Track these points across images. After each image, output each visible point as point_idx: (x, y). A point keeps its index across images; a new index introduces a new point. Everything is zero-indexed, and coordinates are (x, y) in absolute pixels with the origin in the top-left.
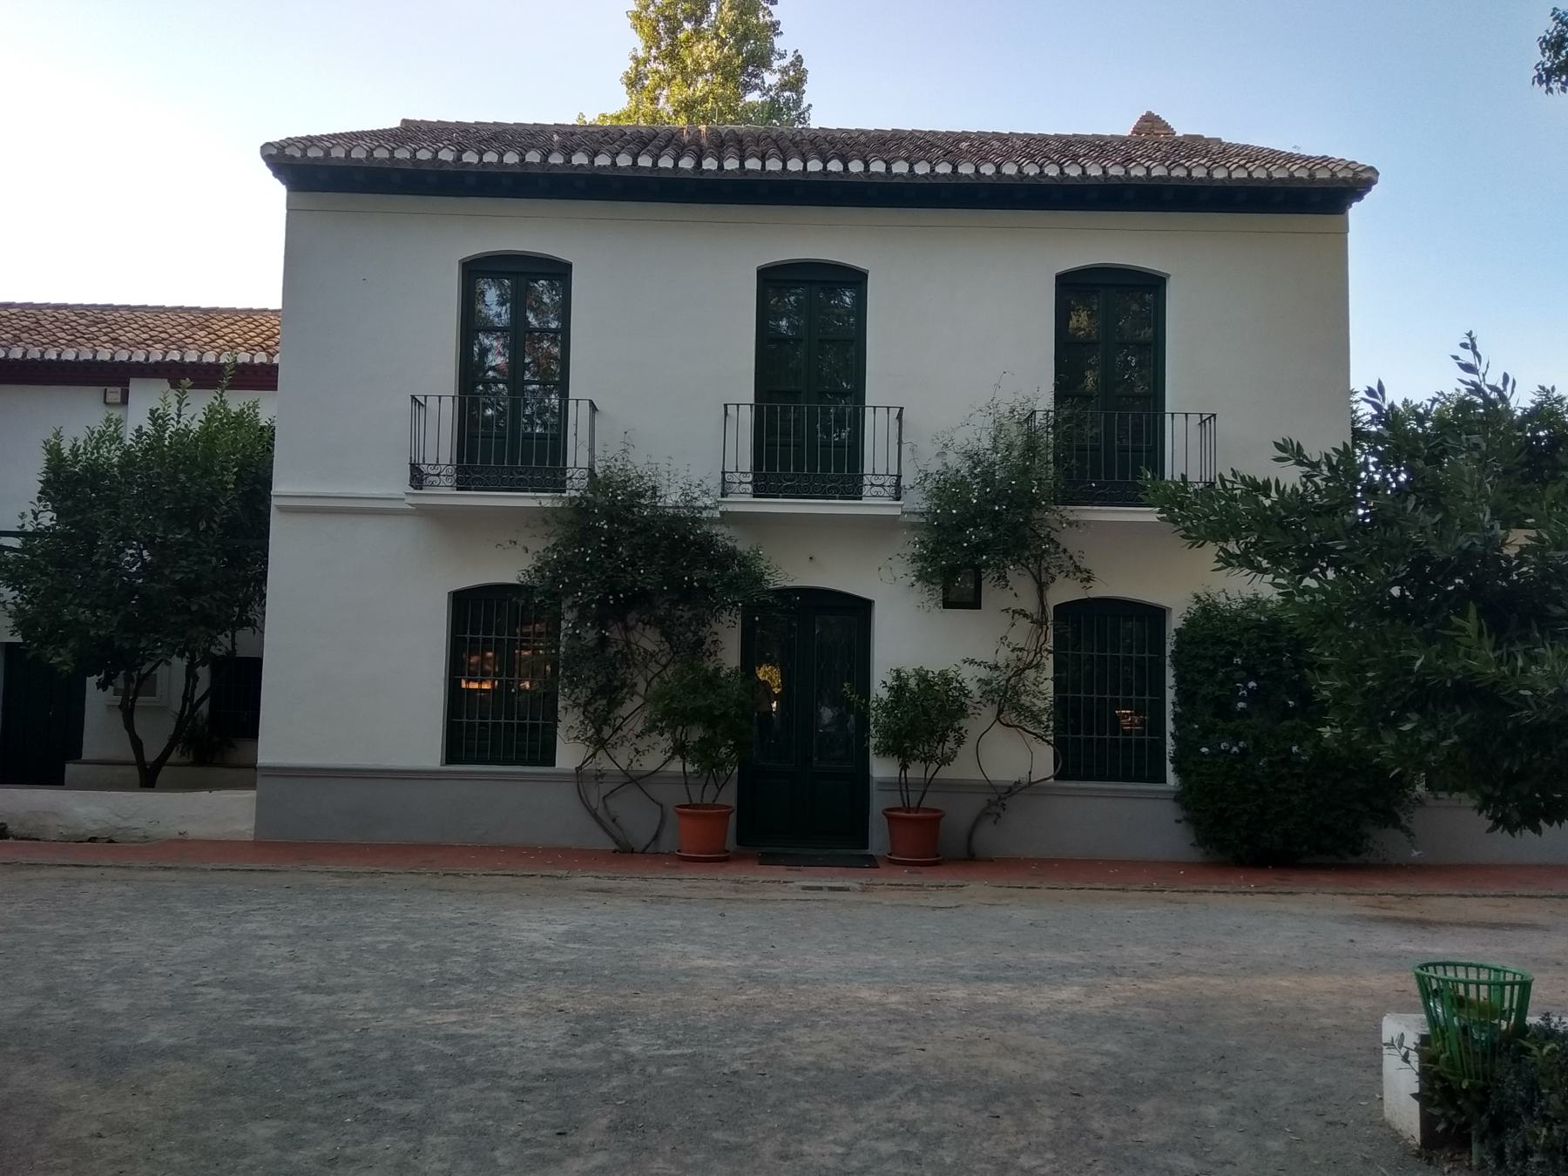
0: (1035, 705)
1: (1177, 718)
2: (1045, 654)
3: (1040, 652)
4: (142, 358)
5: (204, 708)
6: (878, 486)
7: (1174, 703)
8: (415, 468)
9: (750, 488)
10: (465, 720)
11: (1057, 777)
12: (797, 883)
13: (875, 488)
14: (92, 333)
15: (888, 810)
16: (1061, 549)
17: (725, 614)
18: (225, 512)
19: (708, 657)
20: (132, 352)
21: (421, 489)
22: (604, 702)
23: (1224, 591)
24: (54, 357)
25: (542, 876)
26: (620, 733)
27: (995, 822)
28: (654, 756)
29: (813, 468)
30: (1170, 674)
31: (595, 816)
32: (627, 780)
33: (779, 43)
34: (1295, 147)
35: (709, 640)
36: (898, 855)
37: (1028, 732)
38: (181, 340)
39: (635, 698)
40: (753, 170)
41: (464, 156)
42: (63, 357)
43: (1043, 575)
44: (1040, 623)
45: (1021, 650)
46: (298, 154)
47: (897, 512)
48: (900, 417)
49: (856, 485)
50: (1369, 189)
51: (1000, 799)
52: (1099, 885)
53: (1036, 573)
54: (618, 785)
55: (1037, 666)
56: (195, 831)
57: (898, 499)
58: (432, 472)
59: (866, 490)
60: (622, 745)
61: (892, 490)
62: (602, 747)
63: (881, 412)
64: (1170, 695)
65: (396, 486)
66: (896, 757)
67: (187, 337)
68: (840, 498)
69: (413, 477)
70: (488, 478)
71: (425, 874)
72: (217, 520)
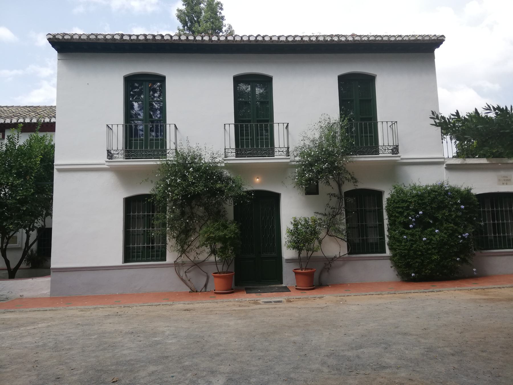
5: (34, 247)
6: (281, 152)
8: (109, 152)
11: (348, 254)
15: (294, 270)
17: (228, 200)
18: (36, 172)
19: (222, 217)
20: (6, 120)
21: (112, 159)
22: (184, 236)
23: (403, 184)
25: (163, 305)
26: (191, 247)
27: (328, 271)
29: (257, 146)
30: (385, 216)
31: (182, 279)
34: (414, 32)
35: (222, 211)
36: (299, 287)
37: (339, 238)
38: (25, 116)
41: (124, 37)
44: (340, 198)
45: (334, 208)
46: (61, 38)
47: (288, 161)
50: (442, 43)
51: (329, 263)
52: (372, 293)
54: (191, 267)
56: (26, 294)
57: (289, 156)
58: (115, 153)
59: (276, 154)
63: (281, 125)
64: (386, 222)
65: (102, 159)
67: (27, 115)
68: (268, 157)
69: (108, 155)
72: (33, 175)
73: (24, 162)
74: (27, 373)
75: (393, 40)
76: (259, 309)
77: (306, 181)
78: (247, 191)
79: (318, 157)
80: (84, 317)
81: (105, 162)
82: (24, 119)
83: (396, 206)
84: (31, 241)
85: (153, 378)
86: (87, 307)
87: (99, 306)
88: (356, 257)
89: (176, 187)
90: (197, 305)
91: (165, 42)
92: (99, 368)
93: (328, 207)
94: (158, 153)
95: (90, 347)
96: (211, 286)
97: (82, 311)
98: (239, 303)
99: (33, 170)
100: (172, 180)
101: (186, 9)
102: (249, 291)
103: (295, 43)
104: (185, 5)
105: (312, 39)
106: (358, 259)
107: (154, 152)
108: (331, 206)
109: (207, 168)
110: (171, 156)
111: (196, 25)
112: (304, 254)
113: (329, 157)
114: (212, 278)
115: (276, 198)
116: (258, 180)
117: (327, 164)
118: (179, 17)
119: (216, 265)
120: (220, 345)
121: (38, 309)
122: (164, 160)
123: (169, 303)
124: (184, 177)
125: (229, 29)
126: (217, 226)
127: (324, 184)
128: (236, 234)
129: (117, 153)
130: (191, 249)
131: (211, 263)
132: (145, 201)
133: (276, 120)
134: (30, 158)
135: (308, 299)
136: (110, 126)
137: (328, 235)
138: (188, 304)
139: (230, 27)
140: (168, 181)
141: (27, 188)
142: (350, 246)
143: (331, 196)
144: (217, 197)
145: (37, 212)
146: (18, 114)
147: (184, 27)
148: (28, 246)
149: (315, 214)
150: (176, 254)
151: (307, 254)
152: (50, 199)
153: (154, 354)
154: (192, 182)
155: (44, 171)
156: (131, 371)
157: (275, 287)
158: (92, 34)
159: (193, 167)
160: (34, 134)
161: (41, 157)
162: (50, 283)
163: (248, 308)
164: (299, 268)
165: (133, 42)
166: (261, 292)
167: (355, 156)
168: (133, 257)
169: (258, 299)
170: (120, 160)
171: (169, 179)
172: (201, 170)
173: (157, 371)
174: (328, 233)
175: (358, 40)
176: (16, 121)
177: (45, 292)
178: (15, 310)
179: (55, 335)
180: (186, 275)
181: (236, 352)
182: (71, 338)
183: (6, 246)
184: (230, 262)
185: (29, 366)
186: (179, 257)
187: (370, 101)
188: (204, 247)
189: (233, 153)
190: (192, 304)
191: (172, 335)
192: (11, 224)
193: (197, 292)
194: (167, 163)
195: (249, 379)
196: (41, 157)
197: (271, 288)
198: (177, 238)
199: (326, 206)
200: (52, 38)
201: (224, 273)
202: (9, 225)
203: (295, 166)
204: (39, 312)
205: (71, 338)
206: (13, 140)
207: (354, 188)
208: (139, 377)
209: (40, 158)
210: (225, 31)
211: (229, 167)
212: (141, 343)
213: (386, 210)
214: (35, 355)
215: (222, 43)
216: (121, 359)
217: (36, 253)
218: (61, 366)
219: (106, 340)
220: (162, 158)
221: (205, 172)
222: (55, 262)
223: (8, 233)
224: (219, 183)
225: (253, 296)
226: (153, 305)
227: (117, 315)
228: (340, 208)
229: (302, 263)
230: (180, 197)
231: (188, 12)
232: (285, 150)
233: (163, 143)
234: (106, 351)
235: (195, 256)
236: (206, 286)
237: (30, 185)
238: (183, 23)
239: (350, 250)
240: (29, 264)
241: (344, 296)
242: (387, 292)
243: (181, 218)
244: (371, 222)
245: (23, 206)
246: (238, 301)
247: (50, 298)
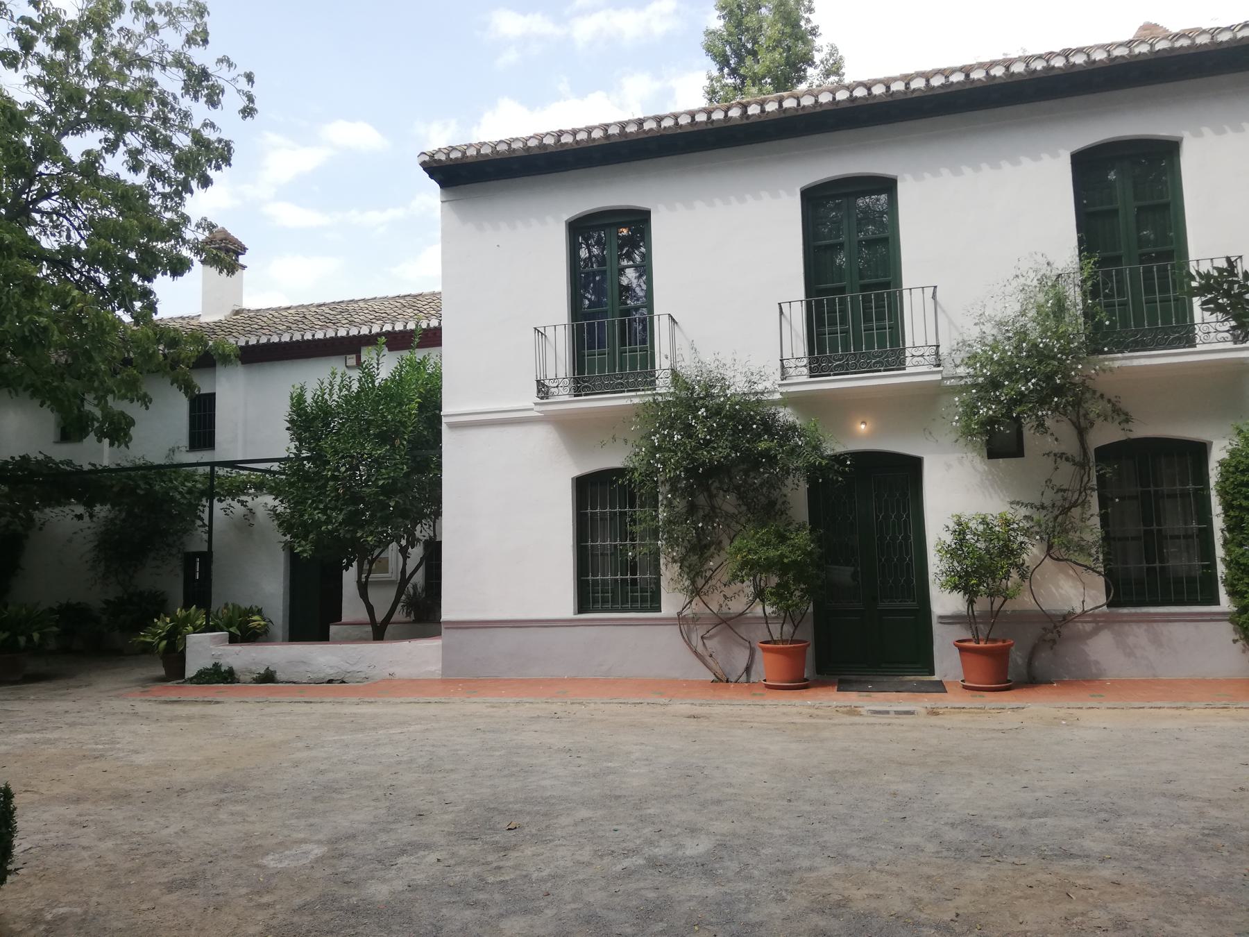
1: (1226, 543)
2: (1089, 492)
3: (1085, 489)
4: (367, 332)
7: (1222, 531)
9: (805, 371)
12: (868, 708)
14: (337, 319)
16: (1098, 394)
18: (412, 432)
21: (547, 398)
24: (310, 338)
31: (696, 653)
33: (818, 42)
35: (780, 502)
38: (394, 317)
40: (790, 108)
41: (562, 138)
42: (316, 337)
43: (1082, 420)
44: (1082, 465)
45: (1064, 491)
46: (443, 158)
47: (938, 377)
48: (934, 296)
51: (1055, 627)
52: (1159, 704)
55: (1084, 503)
56: (401, 672)
57: (939, 365)
58: (552, 385)
59: (908, 360)
60: (712, 593)
61: (932, 359)
62: (698, 594)
64: (1218, 523)
65: (527, 400)
66: (962, 592)
68: (885, 370)
69: (539, 391)
71: (556, 703)
72: (406, 437)
73: (390, 413)
74: (373, 803)
75: (1227, 41)
76: (851, 724)
77: (982, 424)
79: (1011, 364)
80: (492, 717)
81: (532, 406)
83: (1243, 481)
84: (411, 564)
85: (580, 828)
86: (503, 700)
87: (525, 699)
91: (646, 136)
98: (812, 711)
99: (406, 428)
100: (665, 436)
101: (724, 25)
102: (844, 686)
103: (949, 90)
104: (724, 18)
105: (993, 72)
106: (1135, 618)
107: (627, 378)
108: (1058, 485)
109: (737, 407)
110: (663, 385)
111: (749, 61)
112: (982, 604)
113: (1040, 362)
114: (759, 655)
116: (863, 426)
117: (1033, 381)
118: (709, 50)
119: (767, 623)
120: (731, 785)
121: (416, 700)
123: (662, 700)
124: (688, 431)
125: (831, 55)
126: (765, 538)
128: (811, 553)
130: (714, 588)
132: (613, 482)
133: (907, 281)
134: (400, 404)
135: (983, 711)
138: (701, 705)
139: (834, 51)
140: (656, 439)
141: (395, 464)
143: (1059, 459)
144: (762, 470)
146: (383, 315)
147: (721, 70)
148: (404, 580)
149: (1013, 506)
150: (682, 598)
151: (992, 603)
152: (437, 484)
154: (704, 439)
156: (545, 815)
158: (501, 141)
159: (706, 407)
160: (406, 354)
161: (420, 400)
164: (970, 637)
166: (874, 689)
167: (1119, 355)
168: (595, 601)
170: (564, 401)
171: (658, 436)
172: (724, 412)
173: (590, 818)
174: (1051, 552)
175: (1121, 56)
177: (433, 668)
178: (377, 699)
179: (433, 746)
181: (758, 800)
182: (459, 752)
183: (367, 578)
184: (799, 618)
187: (1166, 206)
188: (737, 586)
192: (371, 533)
193: (727, 681)
194: (654, 399)
195: (760, 848)
196: (420, 400)
198: (682, 561)
200: (430, 162)
201: (783, 642)
202: (367, 536)
203: (954, 390)
204: (417, 705)
205: (459, 752)
206: (369, 370)
207: (1123, 438)
208: (556, 825)
209: (416, 402)
210: (822, 62)
211: (791, 400)
213: (1218, 491)
214: (391, 777)
215: (771, 117)
216: (535, 794)
217: (423, 591)
220: (643, 390)
221: (733, 416)
222: (450, 610)
224: (765, 440)
226: (628, 703)
228: (1082, 489)
230: (680, 472)
231: (730, 34)
232: (929, 351)
234: (513, 779)
236: (748, 670)
237: (401, 456)
238: (718, 62)
239: (1112, 595)
240: (410, 613)
241: (1081, 708)
242: (1203, 704)
243: (687, 519)
244: (1173, 524)
245: (390, 498)
246: (810, 706)
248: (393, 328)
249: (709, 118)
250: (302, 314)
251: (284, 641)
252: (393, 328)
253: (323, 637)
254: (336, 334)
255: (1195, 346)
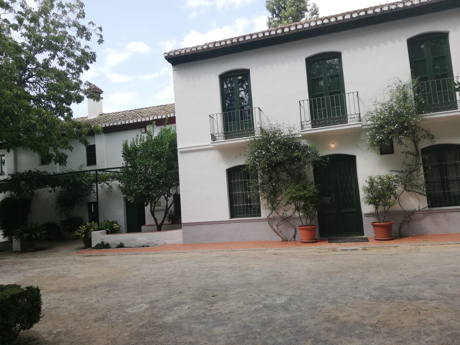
0: (418, 183)
4: (148, 120)
9: (310, 126)
10: (234, 205)
13: (352, 119)
16: (421, 129)
18: (167, 155)
22: (273, 196)
24: (128, 123)
27: (408, 224)
28: (290, 211)
31: (275, 231)
32: (283, 219)
38: (158, 113)
39: (283, 194)
41: (216, 45)
44: (416, 155)
45: (410, 165)
46: (173, 54)
47: (360, 125)
48: (357, 95)
49: (345, 119)
51: (409, 216)
52: (450, 243)
53: (413, 139)
55: (417, 170)
56: (168, 242)
57: (360, 121)
59: (349, 120)
61: (358, 119)
63: (351, 95)
65: (208, 142)
66: (373, 205)
68: (340, 124)
69: (212, 138)
70: (232, 135)
72: (165, 157)
73: (159, 149)
74: (163, 289)
76: (334, 255)
77: (378, 142)
78: (323, 156)
79: (388, 119)
81: (210, 144)
82: (157, 116)
85: (238, 295)
86: (205, 250)
87: (214, 250)
88: (444, 210)
89: (262, 158)
90: (284, 251)
92: (206, 288)
93: (404, 164)
94: (247, 132)
95: (203, 275)
96: (299, 237)
97: (203, 253)
98: (319, 250)
99: (165, 154)
100: (259, 152)
103: (360, 18)
107: (244, 132)
109: (286, 140)
110: (258, 134)
111: (283, 11)
112: (381, 209)
113: (398, 118)
114: (298, 231)
115: (352, 159)
116: (333, 145)
117: (396, 125)
119: (301, 219)
120: (291, 278)
122: (252, 137)
123: (264, 249)
124: (268, 150)
125: (314, 7)
127: (396, 143)
128: (315, 193)
129: (218, 136)
130: (280, 207)
131: (297, 218)
132: (241, 170)
133: (347, 91)
134: (162, 145)
135: (383, 248)
136: (212, 116)
137: (406, 190)
138: (278, 250)
139: (315, 5)
142: (429, 200)
143: (407, 154)
144: (296, 163)
145: (170, 184)
146: (154, 113)
147: (273, 15)
148: (167, 209)
150: (269, 211)
151: (385, 208)
152: (177, 174)
153: (242, 282)
154: (274, 153)
155: (171, 154)
157: (356, 238)
158: (193, 47)
159: (274, 141)
160: (163, 127)
161: (169, 144)
162: (182, 235)
163: (326, 254)
164: (377, 221)
165: (223, 47)
167: (429, 114)
168: (237, 214)
169: (337, 247)
170: (221, 141)
171: (257, 152)
172: (281, 143)
174: (406, 188)
176: (152, 119)
178: (161, 252)
180: (278, 227)
181: (302, 283)
182: (192, 270)
183: (154, 209)
185: (165, 285)
186: (271, 213)
187: (444, 57)
188: (289, 206)
189: (308, 125)
190: (281, 250)
191: (259, 270)
193: (287, 241)
194: (254, 139)
196: (169, 144)
197: (352, 238)
198: (268, 198)
199: (402, 163)
200: (168, 56)
201: (307, 226)
202: (153, 194)
203: (367, 130)
204: (175, 254)
205: (192, 270)
208: (230, 294)
209: (168, 144)
210: (310, 10)
212: (236, 274)
214: (169, 279)
218: (183, 286)
219: (213, 271)
220: (250, 136)
221: (284, 144)
222: (184, 219)
223: (155, 199)
224: (297, 152)
225: (334, 245)
227: (225, 256)
229: (381, 217)
233: (251, 124)
234: (212, 278)
235: (283, 212)
236: (294, 236)
239: (430, 203)
241: (420, 245)
243: (269, 183)
245: (160, 180)
247: (183, 245)
248: (158, 118)
249: (270, 34)
250: (124, 114)
251: (125, 232)
252: (158, 118)
253: (139, 230)
254: (137, 121)
255: (457, 109)
